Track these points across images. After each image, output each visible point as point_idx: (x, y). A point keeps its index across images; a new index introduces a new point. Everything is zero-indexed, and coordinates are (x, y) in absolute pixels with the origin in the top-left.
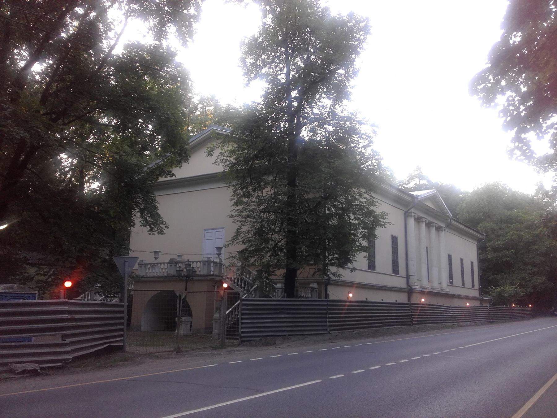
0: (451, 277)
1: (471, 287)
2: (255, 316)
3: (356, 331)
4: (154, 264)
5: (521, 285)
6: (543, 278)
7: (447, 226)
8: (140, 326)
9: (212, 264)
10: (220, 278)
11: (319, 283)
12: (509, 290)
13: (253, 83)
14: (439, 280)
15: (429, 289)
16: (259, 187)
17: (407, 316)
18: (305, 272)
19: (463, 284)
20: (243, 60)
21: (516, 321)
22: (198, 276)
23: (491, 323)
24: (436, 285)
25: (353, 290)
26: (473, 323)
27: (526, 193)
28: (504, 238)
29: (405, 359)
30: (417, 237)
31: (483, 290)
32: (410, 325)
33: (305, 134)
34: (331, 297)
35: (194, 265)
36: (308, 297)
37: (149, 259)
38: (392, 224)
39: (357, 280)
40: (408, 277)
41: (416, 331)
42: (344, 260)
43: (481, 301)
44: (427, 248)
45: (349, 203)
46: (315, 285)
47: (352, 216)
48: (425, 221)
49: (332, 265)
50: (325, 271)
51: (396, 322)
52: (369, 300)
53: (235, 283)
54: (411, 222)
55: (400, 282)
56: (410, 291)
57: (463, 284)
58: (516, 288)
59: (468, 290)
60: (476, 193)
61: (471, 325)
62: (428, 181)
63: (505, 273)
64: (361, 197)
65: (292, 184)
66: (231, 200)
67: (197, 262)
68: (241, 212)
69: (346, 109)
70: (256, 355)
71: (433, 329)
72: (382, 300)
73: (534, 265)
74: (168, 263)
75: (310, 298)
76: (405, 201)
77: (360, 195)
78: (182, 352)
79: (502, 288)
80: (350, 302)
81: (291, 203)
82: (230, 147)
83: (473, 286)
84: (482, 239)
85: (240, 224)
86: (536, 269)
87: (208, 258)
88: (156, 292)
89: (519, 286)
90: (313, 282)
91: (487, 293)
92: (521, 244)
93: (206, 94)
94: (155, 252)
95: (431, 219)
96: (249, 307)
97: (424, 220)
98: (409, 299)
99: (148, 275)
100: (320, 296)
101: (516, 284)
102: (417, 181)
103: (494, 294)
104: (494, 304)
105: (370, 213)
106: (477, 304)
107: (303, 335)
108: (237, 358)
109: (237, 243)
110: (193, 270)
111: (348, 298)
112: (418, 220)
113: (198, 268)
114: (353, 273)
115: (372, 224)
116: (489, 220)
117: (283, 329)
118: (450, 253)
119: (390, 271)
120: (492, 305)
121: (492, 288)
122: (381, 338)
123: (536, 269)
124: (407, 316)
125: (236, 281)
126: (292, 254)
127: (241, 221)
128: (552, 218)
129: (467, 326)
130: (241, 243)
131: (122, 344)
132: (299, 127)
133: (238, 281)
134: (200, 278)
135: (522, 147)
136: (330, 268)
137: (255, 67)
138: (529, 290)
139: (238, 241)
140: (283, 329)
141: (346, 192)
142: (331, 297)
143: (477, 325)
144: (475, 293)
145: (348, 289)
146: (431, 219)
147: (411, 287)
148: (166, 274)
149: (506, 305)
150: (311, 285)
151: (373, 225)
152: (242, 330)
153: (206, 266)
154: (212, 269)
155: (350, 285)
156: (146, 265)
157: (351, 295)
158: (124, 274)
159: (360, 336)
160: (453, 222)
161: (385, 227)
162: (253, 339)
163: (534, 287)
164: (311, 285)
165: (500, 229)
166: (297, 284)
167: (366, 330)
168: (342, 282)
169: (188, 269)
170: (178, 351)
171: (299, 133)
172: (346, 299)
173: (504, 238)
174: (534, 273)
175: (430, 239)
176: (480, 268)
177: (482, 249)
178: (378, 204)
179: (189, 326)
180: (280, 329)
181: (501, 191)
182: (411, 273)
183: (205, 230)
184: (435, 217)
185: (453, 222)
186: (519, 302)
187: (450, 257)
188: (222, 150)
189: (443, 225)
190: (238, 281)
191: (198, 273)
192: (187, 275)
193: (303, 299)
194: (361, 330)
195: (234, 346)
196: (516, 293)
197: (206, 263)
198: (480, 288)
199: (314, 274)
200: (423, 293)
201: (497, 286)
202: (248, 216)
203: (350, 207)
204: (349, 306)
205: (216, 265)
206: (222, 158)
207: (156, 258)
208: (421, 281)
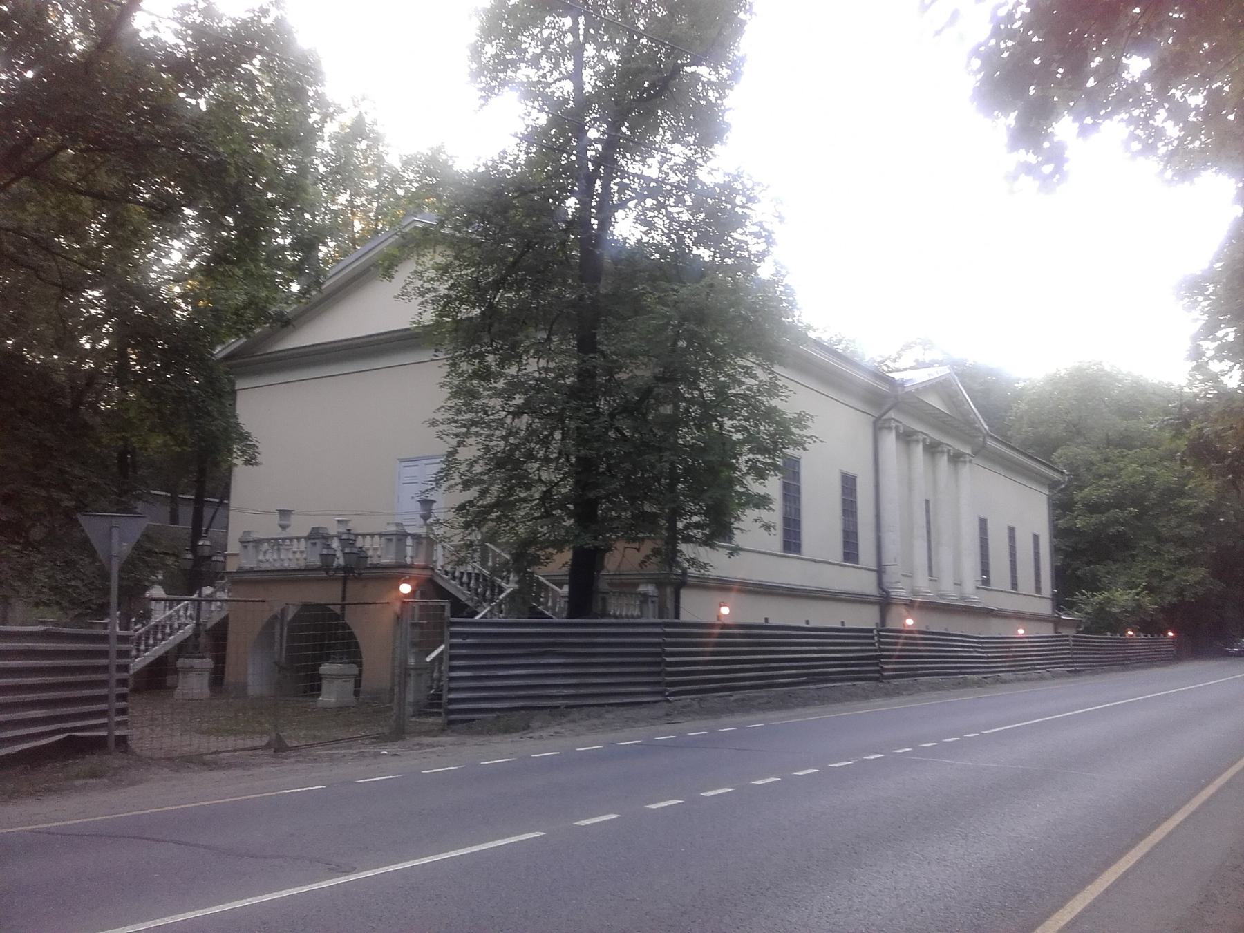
0: (985, 569)
3: (738, 695)
5: (1150, 589)
6: (1200, 573)
7: (976, 453)
8: (245, 686)
9: (409, 541)
11: (660, 585)
12: (1122, 598)
13: (494, 101)
14: (958, 577)
16: (512, 355)
17: (872, 660)
18: (622, 558)
19: (1014, 585)
20: (476, 52)
21: (1135, 668)
22: (375, 567)
24: (947, 590)
25: (733, 596)
26: (1032, 674)
27: (1165, 380)
28: (1114, 482)
29: (876, 753)
30: (903, 475)
31: (1060, 602)
32: (877, 679)
33: (626, 228)
34: (685, 617)
35: (366, 543)
36: (633, 617)
37: (268, 528)
38: (832, 442)
39: (744, 576)
40: (880, 571)
41: (888, 694)
42: (719, 529)
43: (1057, 623)
44: (927, 502)
45: (720, 391)
46: (650, 589)
47: (728, 424)
48: (897, 428)
49: (688, 539)
50: (669, 556)
52: (772, 622)
53: (462, 584)
54: (890, 441)
55: (864, 582)
56: (885, 602)
57: (1014, 585)
58: (1138, 594)
59: (1026, 597)
60: (1054, 381)
63: (1115, 561)
64: (749, 375)
65: (587, 345)
66: (442, 386)
67: (372, 535)
68: (459, 412)
70: (497, 753)
71: (934, 688)
72: (807, 622)
73: (1182, 542)
74: (308, 538)
75: (639, 617)
76: (829, 372)
77: (748, 372)
78: (290, 749)
79: (1107, 594)
80: (724, 626)
81: (585, 388)
82: (435, 257)
83: (1038, 589)
84: (1058, 483)
85: (454, 441)
86: (1183, 553)
87: (397, 525)
89: (1145, 588)
90: (648, 582)
91: (1071, 606)
93: (420, 146)
94: (284, 513)
95: (936, 436)
96: (469, 641)
97: (893, 424)
98: (883, 621)
99: (265, 566)
102: (918, 354)
103: (1089, 609)
105: (770, 415)
106: (1047, 630)
107: (603, 705)
108: (442, 760)
109: (452, 486)
110: (361, 555)
111: (719, 617)
112: (906, 438)
113: (375, 549)
114: (735, 558)
115: (778, 443)
116: (1080, 440)
117: (554, 692)
118: (984, 516)
120: (1082, 632)
121: (1083, 594)
122: (799, 711)
123: (1183, 553)
124: (872, 660)
125: (465, 579)
126: (586, 513)
127: (457, 435)
128: (1192, 415)
129: (1019, 680)
130: (460, 487)
131: (105, 733)
132: (607, 212)
133: (470, 578)
134: (379, 573)
135: (1040, 164)
136: (682, 547)
137: (501, 64)
139: (452, 482)
140: (554, 692)
141: (718, 367)
142: (685, 617)
143: (1042, 678)
145: (717, 596)
146: (936, 436)
147: (888, 593)
148: (302, 564)
149: (1114, 633)
150: (642, 589)
151: (776, 443)
152: (451, 696)
153: (423, 549)
154: (409, 551)
155: (724, 586)
156: (258, 542)
157: (725, 611)
158: (110, 557)
159: (745, 707)
160: (990, 442)
161: (805, 449)
162: (481, 716)
163: (1180, 592)
164: (642, 589)
165: (1106, 460)
166: (603, 585)
167: (762, 692)
169: (347, 550)
170: (279, 748)
171: (605, 223)
172: (713, 620)
173: (1114, 482)
174: (1180, 560)
175: (935, 482)
176: (1055, 550)
177: (1061, 506)
179: (350, 686)
180: (571, 691)
181: (1108, 375)
182: (888, 558)
183: (402, 461)
184: (946, 433)
185: (990, 442)
186: (1149, 626)
187: (983, 523)
188: (418, 264)
189: (967, 450)
190: (470, 578)
191: (375, 561)
192: (352, 569)
193: (626, 621)
194: (753, 693)
195: (429, 733)
196: (1139, 606)
197: (394, 538)
198: (1054, 595)
199: (643, 562)
200: (911, 605)
201: (1095, 587)
202: (474, 423)
203: (723, 402)
205: (419, 543)
206: (418, 283)
207: (283, 527)
208: (909, 579)
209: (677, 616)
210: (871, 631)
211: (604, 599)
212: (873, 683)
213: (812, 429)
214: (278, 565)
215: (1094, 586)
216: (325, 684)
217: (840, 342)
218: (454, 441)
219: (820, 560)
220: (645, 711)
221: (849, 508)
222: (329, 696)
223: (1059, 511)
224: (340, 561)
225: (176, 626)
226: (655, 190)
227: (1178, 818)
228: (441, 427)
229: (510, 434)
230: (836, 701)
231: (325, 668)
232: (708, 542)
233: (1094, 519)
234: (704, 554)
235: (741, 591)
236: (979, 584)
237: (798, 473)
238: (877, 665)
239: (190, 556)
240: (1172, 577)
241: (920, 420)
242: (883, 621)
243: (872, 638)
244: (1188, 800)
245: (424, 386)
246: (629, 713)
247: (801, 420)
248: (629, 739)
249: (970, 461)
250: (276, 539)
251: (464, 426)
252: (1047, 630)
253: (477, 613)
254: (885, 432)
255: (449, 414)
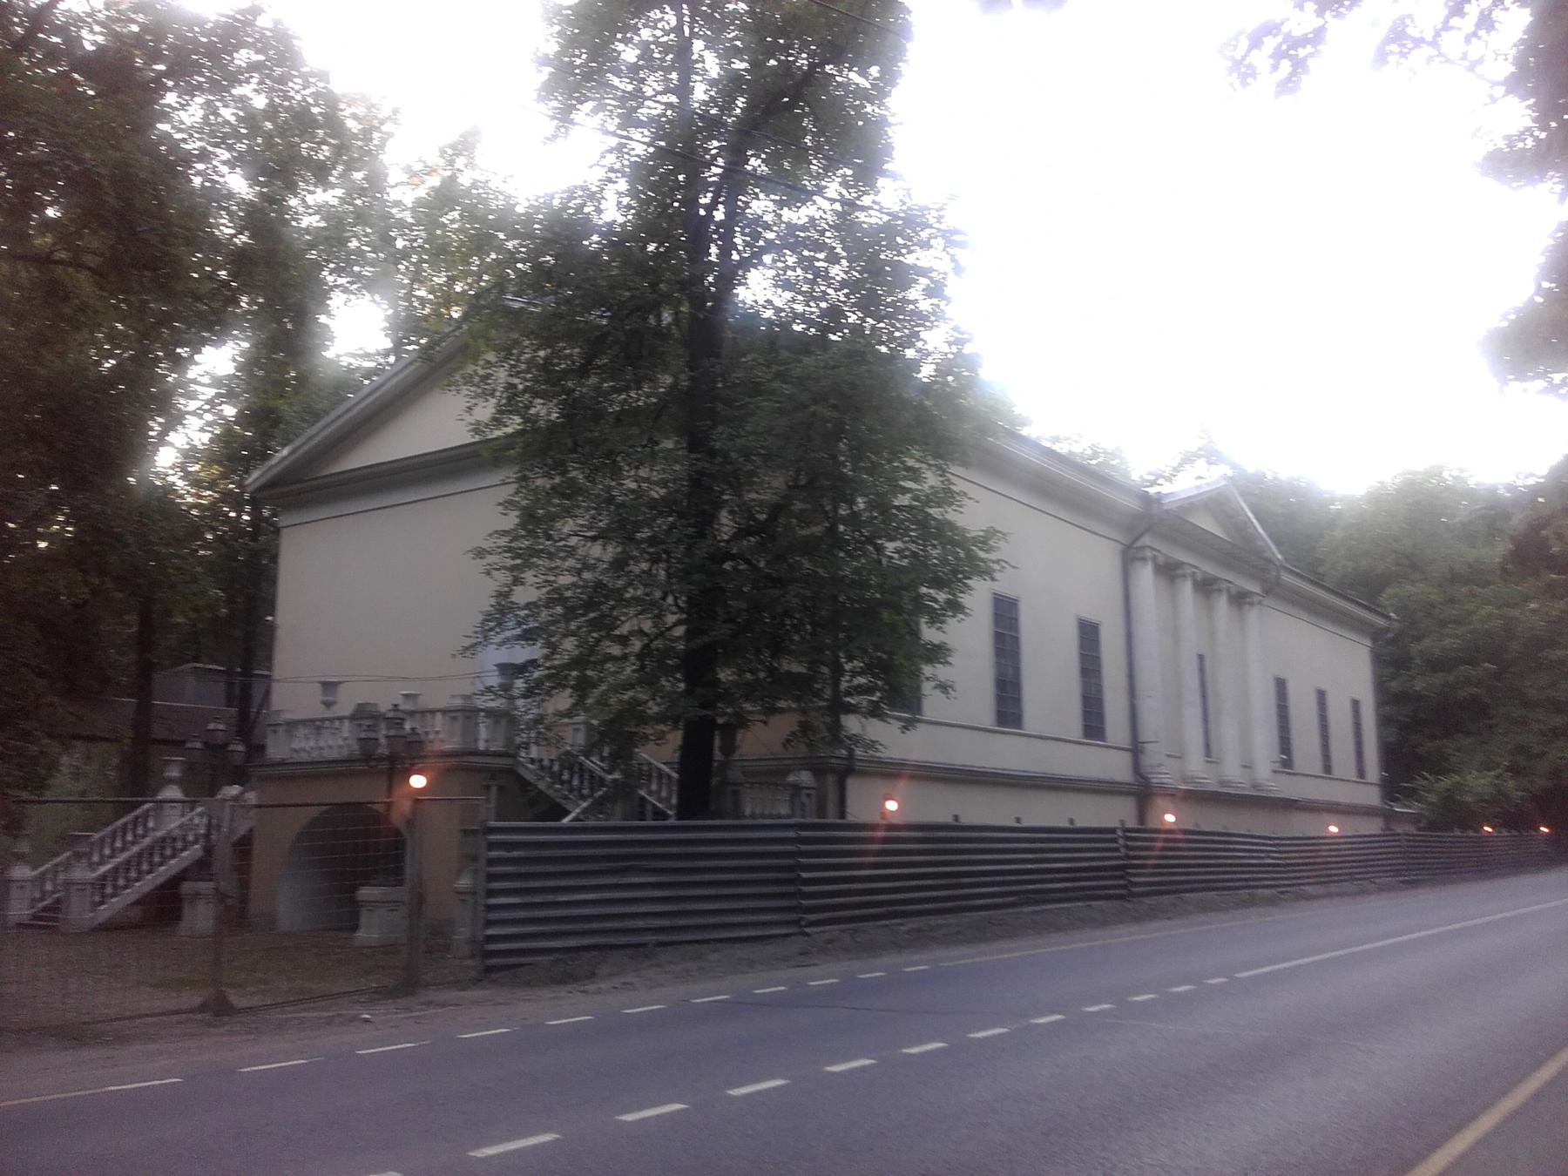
1: (1353, 776)
2: (538, 884)
4: (323, 720)
5: (1515, 771)
7: (1267, 592)
10: (509, 761)
11: (819, 771)
12: (1477, 783)
14: (1248, 757)
15: (1211, 784)
18: (762, 739)
19: (1328, 768)
23: (1413, 884)
24: (1232, 772)
25: (902, 785)
26: (1349, 887)
29: (1054, 1012)
30: (1168, 625)
32: (1121, 897)
33: (759, 291)
36: (780, 816)
38: (1051, 575)
40: (1136, 749)
41: (1138, 919)
42: (898, 695)
43: (1389, 817)
44: (1201, 657)
45: (882, 506)
46: (805, 777)
51: (1066, 890)
54: (1145, 576)
55: (1110, 764)
56: (1143, 792)
57: (1328, 768)
58: (1497, 777)
59: (1344, 785)
60: (1376, 498)
61: (1341, 895)
62: (1234, 466)
63: (1468, 734)
65: (696, 443)
68: (516, 538)
69: (886, 199)
70: (567, 1011)
71: (1205, 908)
72: (1072, 821)
76: (1071, 492)
79: (1457, 778)
81: (696, 503)
83: (1361, 773)
88: (315, 812)
89: (1509, 769)
91: (1411, 794)
92: (1515, 645)
94: (329, 686)
96: (516, 854)
97: (1149, 554)
98: (1142, 818)
99: (304, 757)
100: (822, 812)
101: (1498, 765)
103: (1432, 798)
104: (1432, 826)
105: (944, 534)
106: (1373, 827)
112: (1169, 572)
117: (640, 923)
119: (1075, 728)
120: (1423, 829)
122: (1002, 944)
129: (1330, 895)
138: (1541, 783)
140: (640, 923)
143: (1364, 892)
144: (1370, 796)
145: (880, 786)
146: (1210, 569)
147: (1147, 779)
150: (791, 779)
154: (483, 733)
155: (891, 771)
157: (892, 806)
159: (920, 940)
160: (1286, 578)
161: (993, 579)
162: (523, 960)
164: (791, 779)
166: (735, 774)
167: (951, 919)
168: (880, 762)
170: (219, 1009)
172: (877, 819)
176: (1384, 721)
177: (1392, 661)
178: (966, 501)
180: (666, 922)
181: (1448, 488)
185: (1286, 578)
186: (1515, 820)
187: (1281, 686)
189: (1254, 588)
194: (933, 921)
198: (1383, 779)
201: (1440, 770)
203: (886, 519)
204: (885, 840)
207: (328, 705)
208: (1181, 759)
209: (842, 814)
210: (1113, 831)
211: (736, 793)
212: (1116, 903)
213: (1003, 551)
214: (315, 755)
215: (1439, 766)
216: (364, 918)
217: (1095, 455)
218: (503, 578)
219: (1049, 734)
220: (770, 949)
221: (1090, 668)
222: (370, 931)
223: (1392, 670)
224: (383, 750)
225: (191, 838)
226: (793, 239)
227: (1486, 1122)
228: (491, 559)
229: (587, 567)
230: (1059, 929)
231: (365, 893)
232: (875, 712)
233: (1439, 679)
234: (875, 730)
235: (913, 777)
236: (1277, 766)
237: (1016, 620)
238: (1122, 877)
239: (241, 748)
240: (1543, 754)
241: (1189, 548)
242: (1142, 818)
243: (1115, 840)
244: (1503, 1094)
245: (485, 510)
246: (741, 951)
247: (984, 541)
248: (710, 993)
249: (1260, 603)
250: (313, 721)
251: (519, 556)
252: (1373, 827)
253: (567, 813)
254: (1138, 564)
255: (503, 541)
